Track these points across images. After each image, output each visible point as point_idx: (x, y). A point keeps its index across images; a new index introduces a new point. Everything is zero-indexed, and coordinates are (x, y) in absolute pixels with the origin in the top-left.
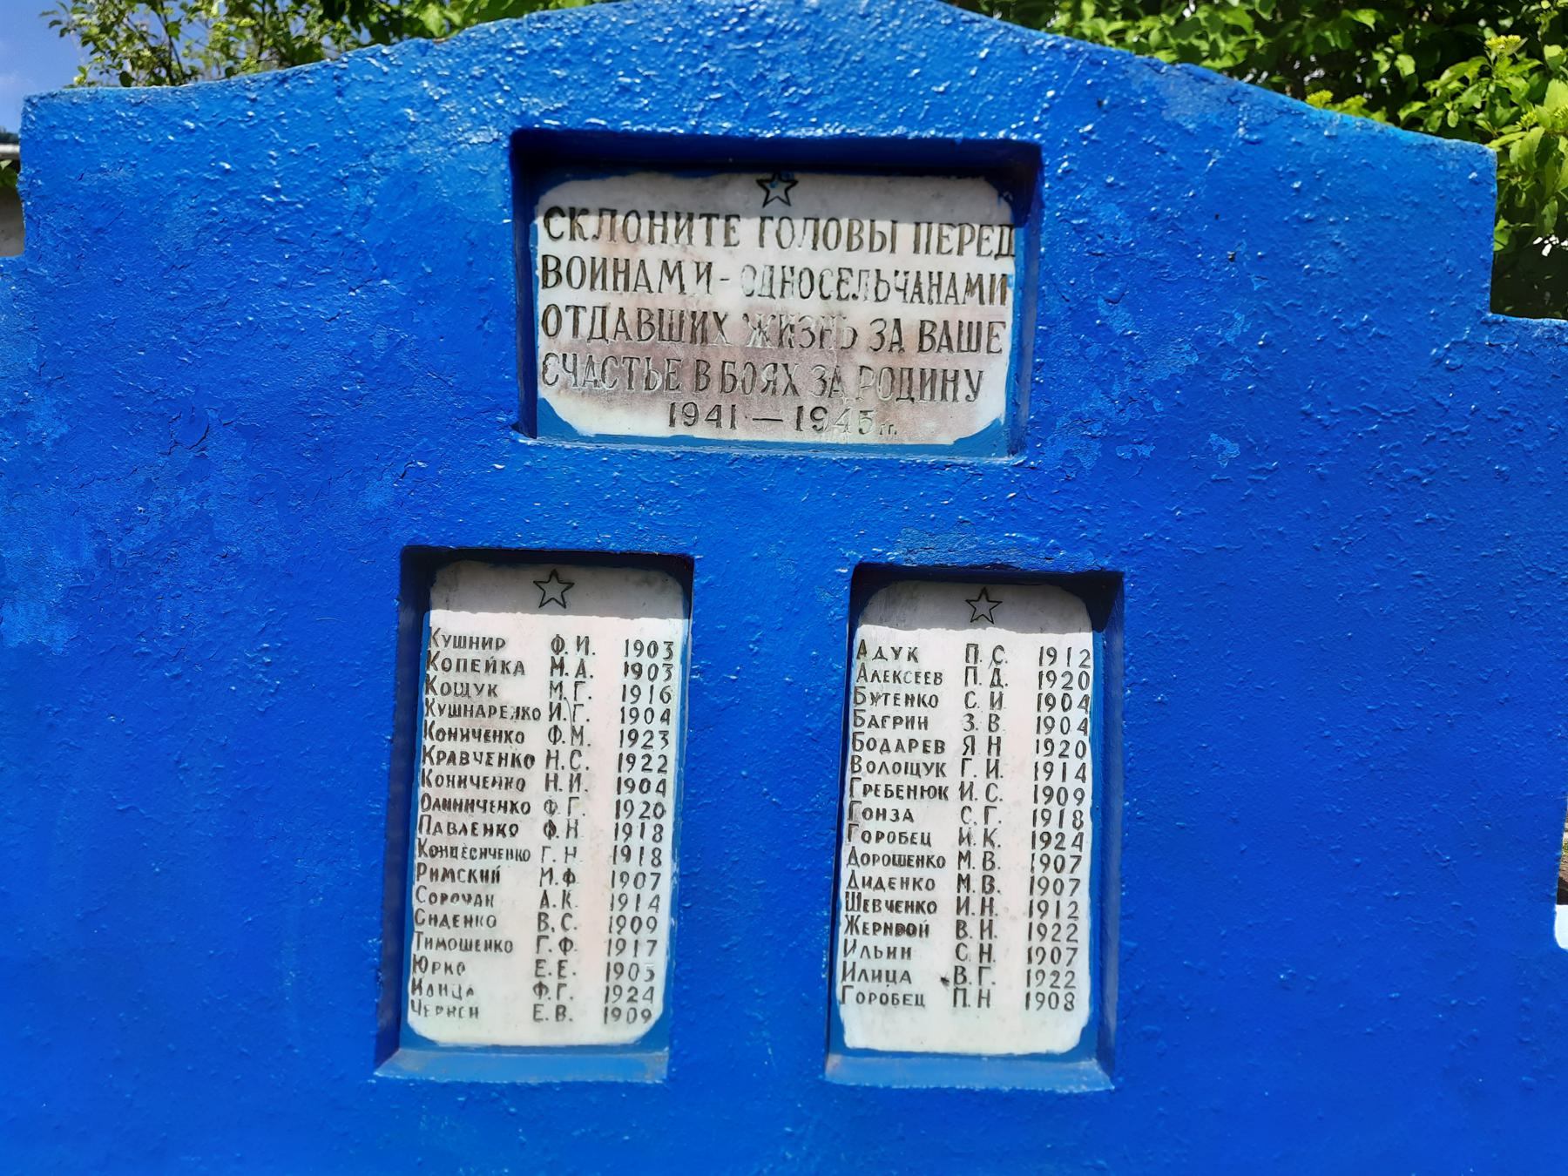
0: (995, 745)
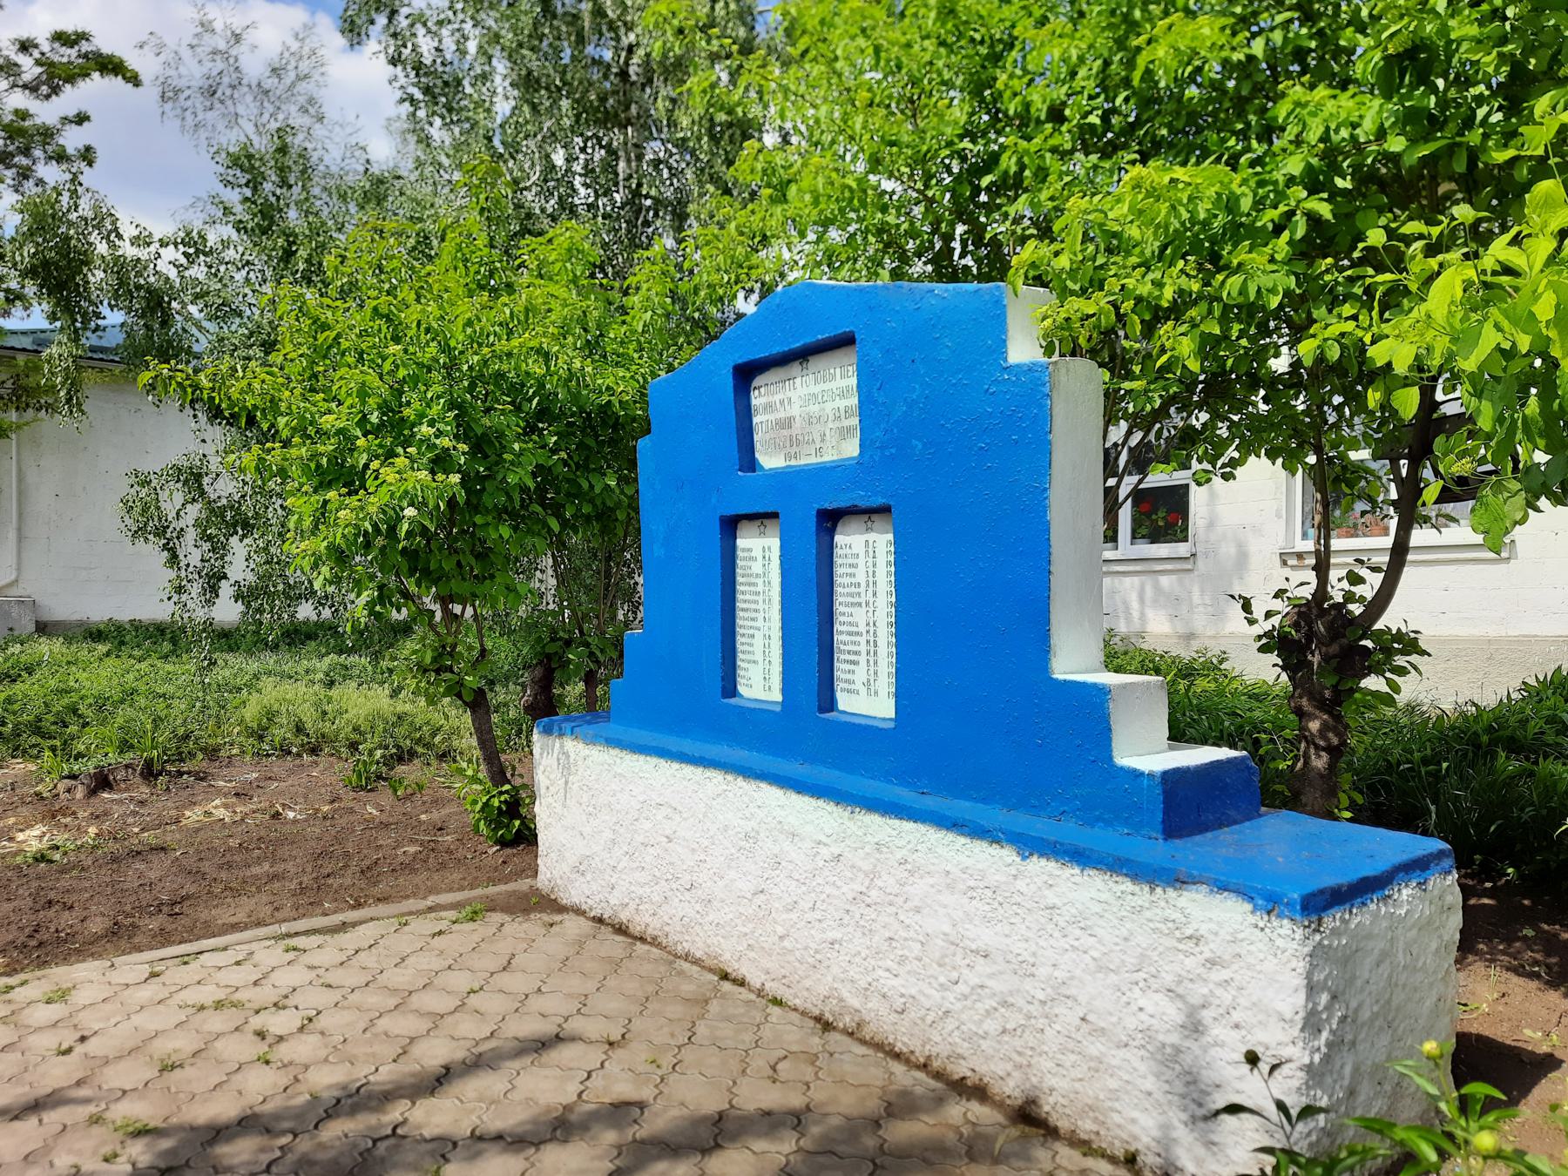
0: (875, 583)
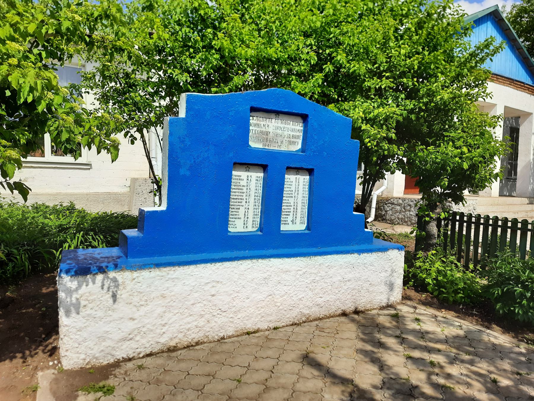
0: (298, 191)
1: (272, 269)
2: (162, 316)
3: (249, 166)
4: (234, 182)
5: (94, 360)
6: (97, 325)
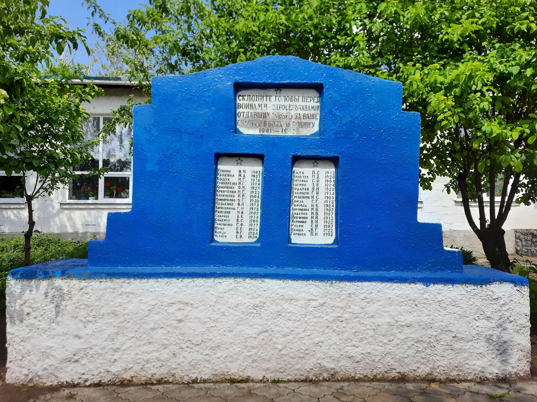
0: (318, 189)
1: (266, 294)
2: (113, 339)
3: (241, 159)
4: (221, 179)
5: (37, 379)
6: (40, 337)
